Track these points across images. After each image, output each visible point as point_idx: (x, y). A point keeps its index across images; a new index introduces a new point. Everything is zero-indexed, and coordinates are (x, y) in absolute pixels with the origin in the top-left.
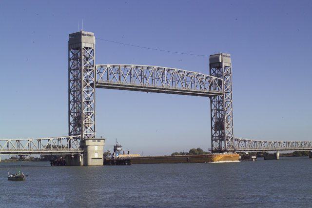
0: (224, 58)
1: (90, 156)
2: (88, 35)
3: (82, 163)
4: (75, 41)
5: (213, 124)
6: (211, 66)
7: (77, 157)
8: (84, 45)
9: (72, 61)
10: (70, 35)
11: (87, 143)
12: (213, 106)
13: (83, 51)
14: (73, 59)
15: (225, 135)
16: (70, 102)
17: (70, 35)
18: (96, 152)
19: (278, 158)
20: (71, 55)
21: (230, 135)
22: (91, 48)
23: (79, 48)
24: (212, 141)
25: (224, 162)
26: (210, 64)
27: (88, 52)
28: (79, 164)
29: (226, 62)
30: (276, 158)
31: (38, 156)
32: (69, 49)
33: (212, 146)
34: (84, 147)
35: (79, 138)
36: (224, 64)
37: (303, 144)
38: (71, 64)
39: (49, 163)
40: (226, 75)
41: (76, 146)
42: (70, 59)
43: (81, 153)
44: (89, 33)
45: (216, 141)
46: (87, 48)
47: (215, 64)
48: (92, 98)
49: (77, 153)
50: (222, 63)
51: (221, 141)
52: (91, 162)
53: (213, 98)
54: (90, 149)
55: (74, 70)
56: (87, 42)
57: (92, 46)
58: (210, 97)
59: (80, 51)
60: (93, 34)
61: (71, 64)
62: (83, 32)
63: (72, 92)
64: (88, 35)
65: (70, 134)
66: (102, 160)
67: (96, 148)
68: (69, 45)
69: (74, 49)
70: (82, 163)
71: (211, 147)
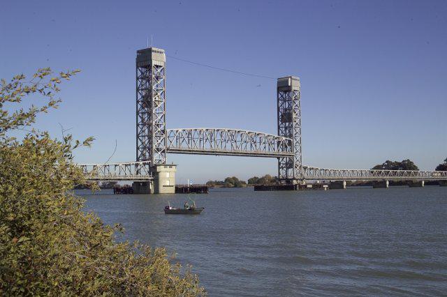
0: (293, 81)
1: (162, 183)
2: (158, 52)
3: (152, 191)
4: (144, 59)
5: (280, 114)
6: (279, 89)
7: (146, 184)
8: (154, 63)
9: (140, 80)
10: (138, 52)
11: (158, 169)
12: (280, 96)
13: (153, 69)
14: (142, 78)
15: (293, 163)
16: (138, 125)
17: (138, 52)
18: (168, 179)
19: (345, 187)
20: (139, 73)
21: (298, 163)
22: (160, 66)
23: (148, 67)
24: (279, 168)
25: (411, 271)
26: (278, 88)
27: (159, 70)
28: (148, 192)
29: (296, 85)
30: (342, 187)
31: (130, 183)
32: (137, 67)
33: (279, 174)
34: (153, 171)
35: (147, 164)
36: (293, 88)
37: (332, 172)
38: (139, 83)
39: (111, 191)
40: (296, 99)
41: (144, 173)
42: (138, 78)
43: (152, 180)
44: (160, 50)
45: (283, 168)
46: (157, 66)
47: (284, 88)
48: (162, 120)
49: (147, 179)
50: (291, 86)
51: (288, 168)
52: (162, 190)
53: (281, 159)
54: (161, 175)
55: (142, 90)
56: (158, 59)
57: (162, 64)
58: (278, 158)
59: (150, 70)
60: (163, 50)
61: (139, 83)
62: (153, 49)
63: (140, 115)
64: (158, 52)
65: (138, 160)
66: (174, 188)
67: (168, 175)
68: (137, 63)
69: (142, 67)
70: (152, 191)
71: (277, 175)
